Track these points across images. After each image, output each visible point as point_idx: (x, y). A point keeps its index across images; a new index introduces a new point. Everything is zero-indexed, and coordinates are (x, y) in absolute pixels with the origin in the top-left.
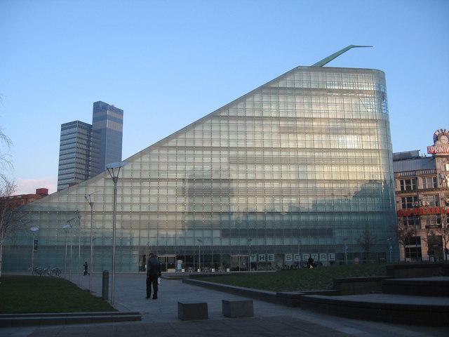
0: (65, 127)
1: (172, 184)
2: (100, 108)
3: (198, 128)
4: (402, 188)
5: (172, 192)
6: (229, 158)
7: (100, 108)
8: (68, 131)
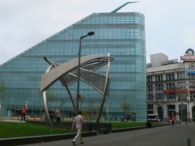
4: (167, 79)
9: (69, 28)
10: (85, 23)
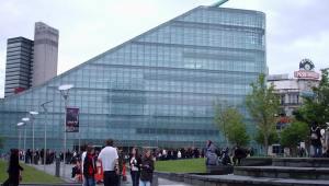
0: (11, 41)
1: (100, 93)
2: (41, 28)
3: (121, 51)
5: (99, 99)
6: (144, 74)
7: (41, 28)
8: (12, 45)
9: (164, 26)
10: (186, 19)
